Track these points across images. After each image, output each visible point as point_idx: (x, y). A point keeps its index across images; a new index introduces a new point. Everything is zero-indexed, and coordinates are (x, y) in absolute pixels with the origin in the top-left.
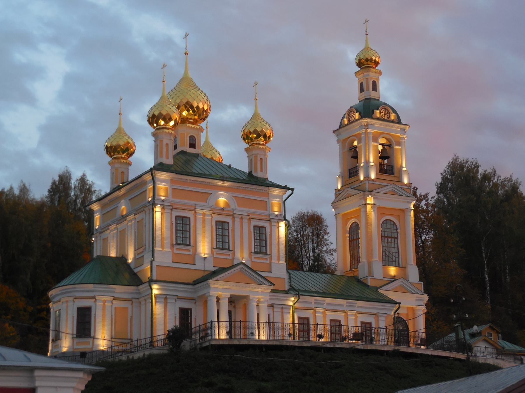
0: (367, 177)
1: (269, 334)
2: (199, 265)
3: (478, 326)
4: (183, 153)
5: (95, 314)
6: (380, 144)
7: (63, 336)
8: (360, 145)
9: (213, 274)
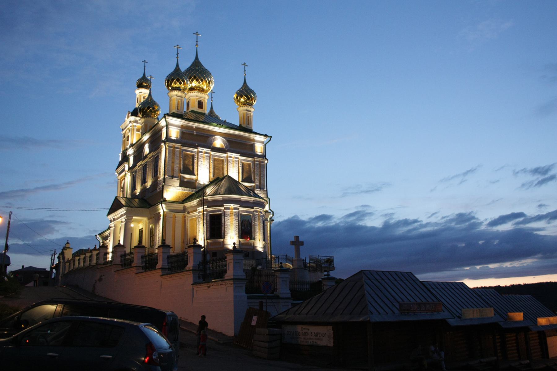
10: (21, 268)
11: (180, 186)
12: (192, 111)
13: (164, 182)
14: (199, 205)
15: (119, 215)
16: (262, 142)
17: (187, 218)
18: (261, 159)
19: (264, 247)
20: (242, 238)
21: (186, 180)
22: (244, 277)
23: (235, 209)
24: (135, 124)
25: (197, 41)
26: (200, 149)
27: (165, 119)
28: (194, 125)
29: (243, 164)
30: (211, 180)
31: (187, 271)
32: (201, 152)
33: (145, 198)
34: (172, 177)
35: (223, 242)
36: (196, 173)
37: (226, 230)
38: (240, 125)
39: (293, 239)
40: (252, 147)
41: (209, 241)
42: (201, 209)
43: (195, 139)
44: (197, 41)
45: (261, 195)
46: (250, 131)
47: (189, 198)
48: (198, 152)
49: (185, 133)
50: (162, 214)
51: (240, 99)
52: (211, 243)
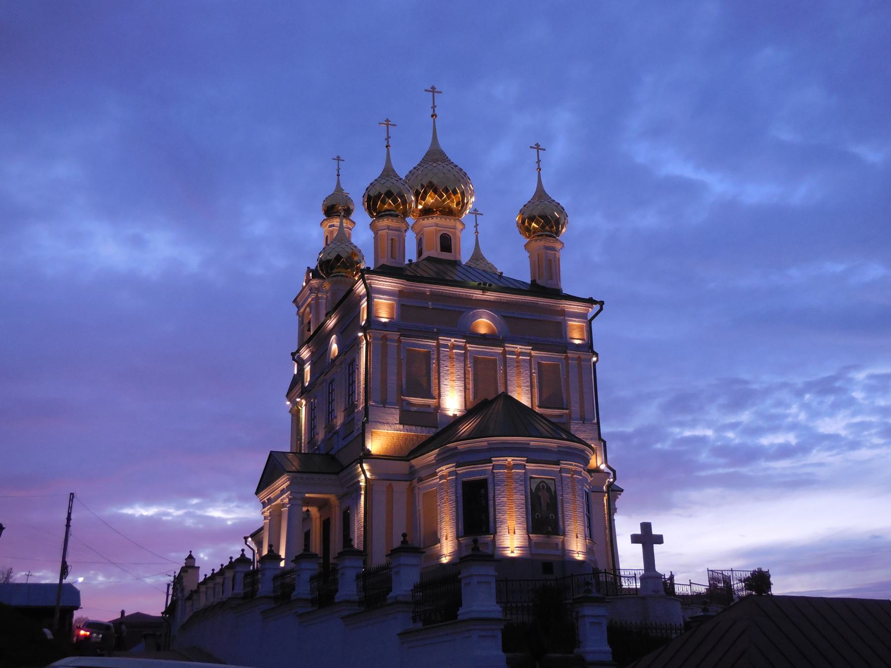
10: (119, 616)
11: (400, 423)
12: (429, 259)
13: (367, 415)
14: (441, 461)
15: (278, 491)
16: (581, 316)
17: (416, 491)
18: (583, 355)
19: (589, 551)
20: (532, 533)
21: (414, 409)
22: (500, 616)
23: (516, 466)
25: (434, 107)
26: (443, 340)
29: (540, 365)
30: (470, 406)
31: (389, 605)
32: (446, 346)
33: (332, 452)
34: (384, 403)
35: (494, 541)
36: (435, 393)
37: (499, 516)
38: (533, 281)
39: (655, 531)
40: (561, 329)
42: (444, 470)
43: (415, 319)
44: (434, 107)
45: (581, 436)
46: (557, 294)
47: (421, 448)
50: (363, 484)
51: (530, 225)
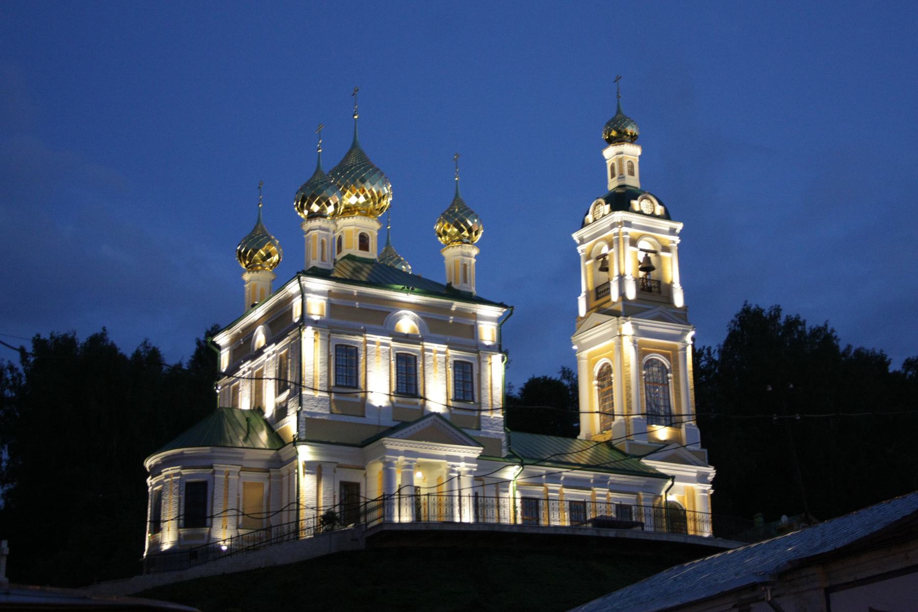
0: (622, 295)
1: (476, 516)
2: (370, 419)
3: (788, 516)
4: (350, 257)
5: (213, 493)
6: (641, 250)
7: (165, 526)
8: (612, 250)
9: (390, 431)
20: (185, 527)
24: (625, 229)
26: (371, 337)
27: (299, 282)
28: (356, 289)
40: (473, 331)
41: (182, 531)
48: (367, 342)
49: (335, 305)
52: (186, 536)
